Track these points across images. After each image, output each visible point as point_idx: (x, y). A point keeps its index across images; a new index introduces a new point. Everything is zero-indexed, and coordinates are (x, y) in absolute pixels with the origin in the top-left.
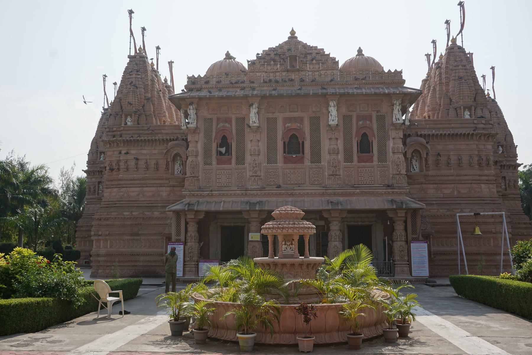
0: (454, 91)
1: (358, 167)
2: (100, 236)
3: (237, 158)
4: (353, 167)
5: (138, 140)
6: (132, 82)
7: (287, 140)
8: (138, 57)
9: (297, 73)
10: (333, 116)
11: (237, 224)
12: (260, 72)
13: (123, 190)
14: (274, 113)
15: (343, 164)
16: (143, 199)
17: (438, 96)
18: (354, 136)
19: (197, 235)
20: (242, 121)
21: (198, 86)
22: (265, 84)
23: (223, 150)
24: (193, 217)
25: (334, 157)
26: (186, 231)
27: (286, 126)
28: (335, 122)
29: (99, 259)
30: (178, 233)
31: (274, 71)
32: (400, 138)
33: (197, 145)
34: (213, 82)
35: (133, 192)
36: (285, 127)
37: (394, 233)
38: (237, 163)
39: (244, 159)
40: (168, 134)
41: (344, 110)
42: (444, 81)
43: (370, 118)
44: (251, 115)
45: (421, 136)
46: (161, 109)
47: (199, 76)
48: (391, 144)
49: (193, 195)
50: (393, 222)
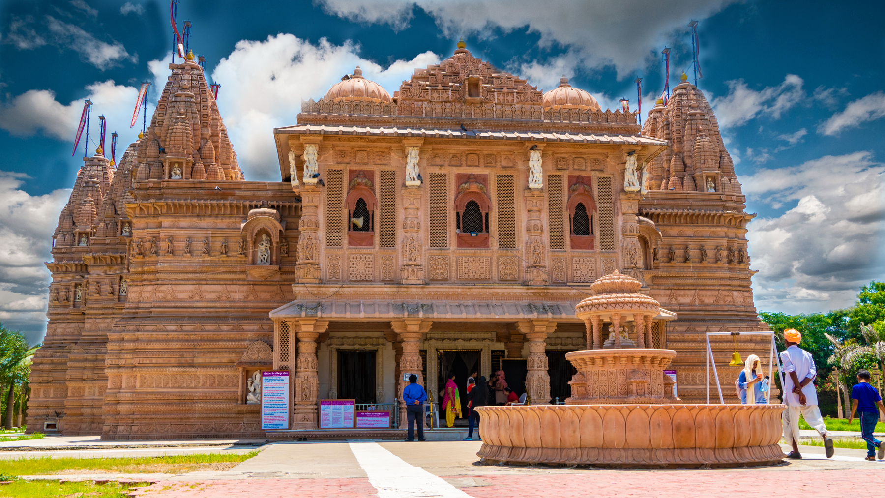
3: (382, 236)
14: (442, 166)
18: (564, 208)
30: (284, 356)
35: (183, 291)
38: (383, 244)
39: (393, 236)
41: (550, 165)
45: (646, 215)
46: (228, 156)
48: (619, 221)
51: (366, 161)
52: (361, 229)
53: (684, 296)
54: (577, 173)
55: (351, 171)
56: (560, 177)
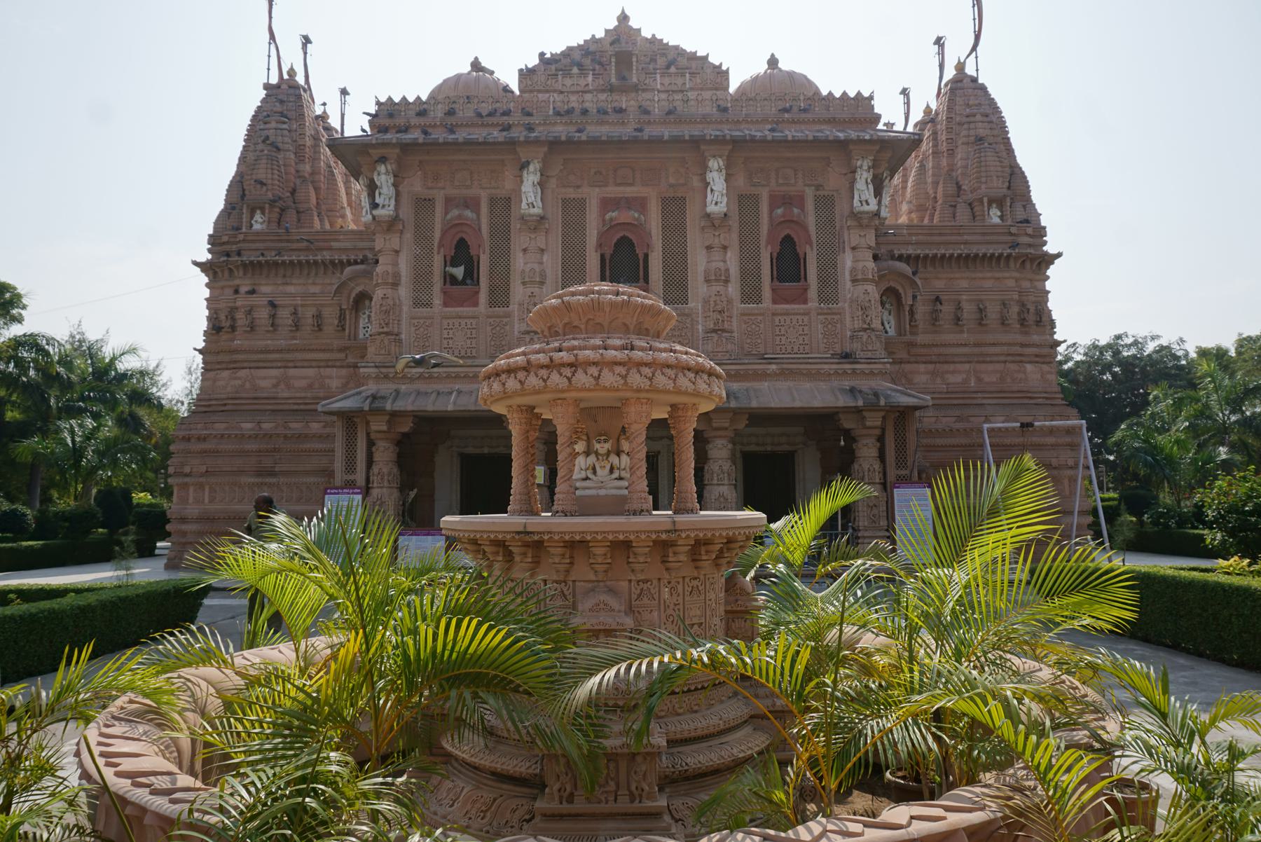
0: (966, 167)
1: (774, 314)
2: (186, 475)
3: (492, 291)
4: (762, 314)
5: (276, 264)
6: (267, 138)
7: (608, 251)
8: (284, 86)
9: (633, 95)
10: (718, 195)
11: (497, 450)
12: (547, 91)
13: (242, 373)
14: (578, 187)
15: (739, 306)
16: (286, 395)
17: (930, 180)
19: (395, 470)
20: (504, 205)
21: (400, 121)
22: (558, 119)
23: (459, 272)
24: (385, 428)
25: (718, 288)
26: (370, 462)
27: (607, 217)
28: (722, 208)
29: (184, 527)
30: (350, 467)
31: (579, 89)
32: (870, 248)
33: (399, 260)
34: (439, 112)
35: (265, 378)
36: (604, 220)
37: (856, 466)
38: (492, 303)
40: (346, 249)
41: (740, 181)
42: (943, 147)
43: (800, 201)
44: (523, 189)
45: (900, 258)
47: (404, 98)
48: (847, 261)
49: (386, 377)
50: (850, 438)
51: (468, 183)
52: (463, 282)
53: (953, 372)
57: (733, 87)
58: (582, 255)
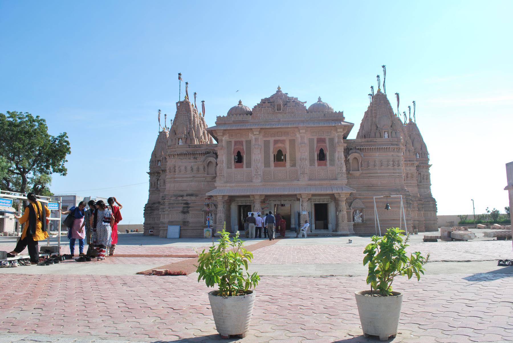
7: (276, 153)
33: (223, 157)
38: (247, 167)
54: (320, 137)
55: (235, 142)
56: (313, 139)
57: (307, 108)
58: (269, 154)
